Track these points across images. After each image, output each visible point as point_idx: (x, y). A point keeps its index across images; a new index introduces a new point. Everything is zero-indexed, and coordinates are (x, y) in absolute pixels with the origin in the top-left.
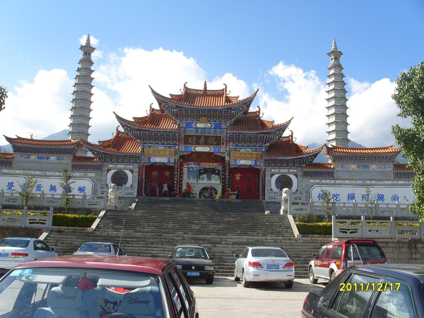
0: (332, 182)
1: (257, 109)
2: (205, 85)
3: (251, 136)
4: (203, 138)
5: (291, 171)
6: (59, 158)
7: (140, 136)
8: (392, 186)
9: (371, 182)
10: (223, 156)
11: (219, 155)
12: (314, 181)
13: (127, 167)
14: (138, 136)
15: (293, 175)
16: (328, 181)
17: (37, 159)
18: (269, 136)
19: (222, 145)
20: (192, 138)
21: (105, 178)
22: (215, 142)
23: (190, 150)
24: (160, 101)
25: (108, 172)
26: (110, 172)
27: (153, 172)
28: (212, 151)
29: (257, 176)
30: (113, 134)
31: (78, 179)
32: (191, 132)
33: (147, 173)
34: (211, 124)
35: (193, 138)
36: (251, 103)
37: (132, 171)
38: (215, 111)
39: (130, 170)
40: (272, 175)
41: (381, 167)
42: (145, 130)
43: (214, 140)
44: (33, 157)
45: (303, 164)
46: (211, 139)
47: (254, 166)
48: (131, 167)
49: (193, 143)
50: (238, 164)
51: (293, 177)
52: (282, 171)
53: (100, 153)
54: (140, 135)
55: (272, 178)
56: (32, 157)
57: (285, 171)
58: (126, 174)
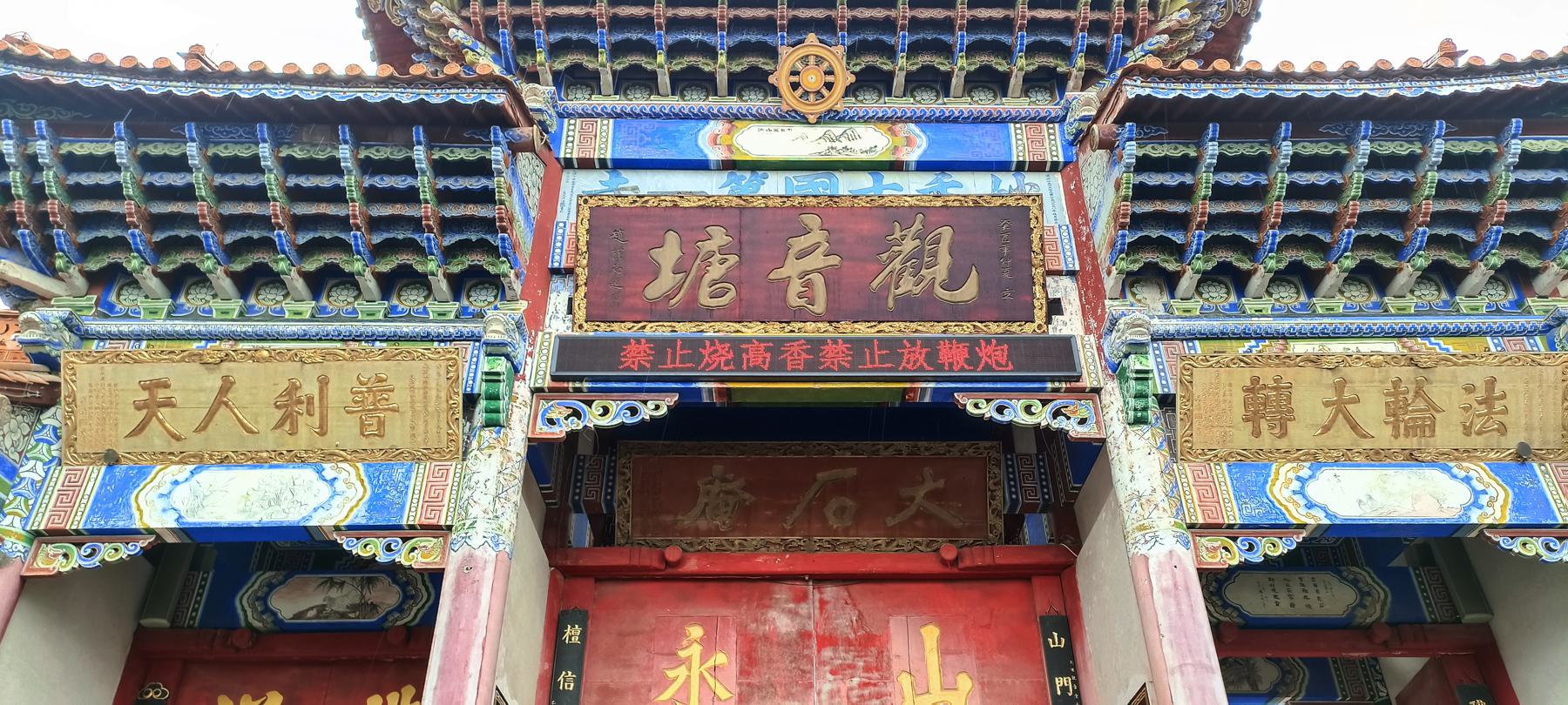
11: (1024, 419)
19: (1040, 314)
43: (944, 259)
46: (909, 245)
49: (705, 299)
54: (38, 193)
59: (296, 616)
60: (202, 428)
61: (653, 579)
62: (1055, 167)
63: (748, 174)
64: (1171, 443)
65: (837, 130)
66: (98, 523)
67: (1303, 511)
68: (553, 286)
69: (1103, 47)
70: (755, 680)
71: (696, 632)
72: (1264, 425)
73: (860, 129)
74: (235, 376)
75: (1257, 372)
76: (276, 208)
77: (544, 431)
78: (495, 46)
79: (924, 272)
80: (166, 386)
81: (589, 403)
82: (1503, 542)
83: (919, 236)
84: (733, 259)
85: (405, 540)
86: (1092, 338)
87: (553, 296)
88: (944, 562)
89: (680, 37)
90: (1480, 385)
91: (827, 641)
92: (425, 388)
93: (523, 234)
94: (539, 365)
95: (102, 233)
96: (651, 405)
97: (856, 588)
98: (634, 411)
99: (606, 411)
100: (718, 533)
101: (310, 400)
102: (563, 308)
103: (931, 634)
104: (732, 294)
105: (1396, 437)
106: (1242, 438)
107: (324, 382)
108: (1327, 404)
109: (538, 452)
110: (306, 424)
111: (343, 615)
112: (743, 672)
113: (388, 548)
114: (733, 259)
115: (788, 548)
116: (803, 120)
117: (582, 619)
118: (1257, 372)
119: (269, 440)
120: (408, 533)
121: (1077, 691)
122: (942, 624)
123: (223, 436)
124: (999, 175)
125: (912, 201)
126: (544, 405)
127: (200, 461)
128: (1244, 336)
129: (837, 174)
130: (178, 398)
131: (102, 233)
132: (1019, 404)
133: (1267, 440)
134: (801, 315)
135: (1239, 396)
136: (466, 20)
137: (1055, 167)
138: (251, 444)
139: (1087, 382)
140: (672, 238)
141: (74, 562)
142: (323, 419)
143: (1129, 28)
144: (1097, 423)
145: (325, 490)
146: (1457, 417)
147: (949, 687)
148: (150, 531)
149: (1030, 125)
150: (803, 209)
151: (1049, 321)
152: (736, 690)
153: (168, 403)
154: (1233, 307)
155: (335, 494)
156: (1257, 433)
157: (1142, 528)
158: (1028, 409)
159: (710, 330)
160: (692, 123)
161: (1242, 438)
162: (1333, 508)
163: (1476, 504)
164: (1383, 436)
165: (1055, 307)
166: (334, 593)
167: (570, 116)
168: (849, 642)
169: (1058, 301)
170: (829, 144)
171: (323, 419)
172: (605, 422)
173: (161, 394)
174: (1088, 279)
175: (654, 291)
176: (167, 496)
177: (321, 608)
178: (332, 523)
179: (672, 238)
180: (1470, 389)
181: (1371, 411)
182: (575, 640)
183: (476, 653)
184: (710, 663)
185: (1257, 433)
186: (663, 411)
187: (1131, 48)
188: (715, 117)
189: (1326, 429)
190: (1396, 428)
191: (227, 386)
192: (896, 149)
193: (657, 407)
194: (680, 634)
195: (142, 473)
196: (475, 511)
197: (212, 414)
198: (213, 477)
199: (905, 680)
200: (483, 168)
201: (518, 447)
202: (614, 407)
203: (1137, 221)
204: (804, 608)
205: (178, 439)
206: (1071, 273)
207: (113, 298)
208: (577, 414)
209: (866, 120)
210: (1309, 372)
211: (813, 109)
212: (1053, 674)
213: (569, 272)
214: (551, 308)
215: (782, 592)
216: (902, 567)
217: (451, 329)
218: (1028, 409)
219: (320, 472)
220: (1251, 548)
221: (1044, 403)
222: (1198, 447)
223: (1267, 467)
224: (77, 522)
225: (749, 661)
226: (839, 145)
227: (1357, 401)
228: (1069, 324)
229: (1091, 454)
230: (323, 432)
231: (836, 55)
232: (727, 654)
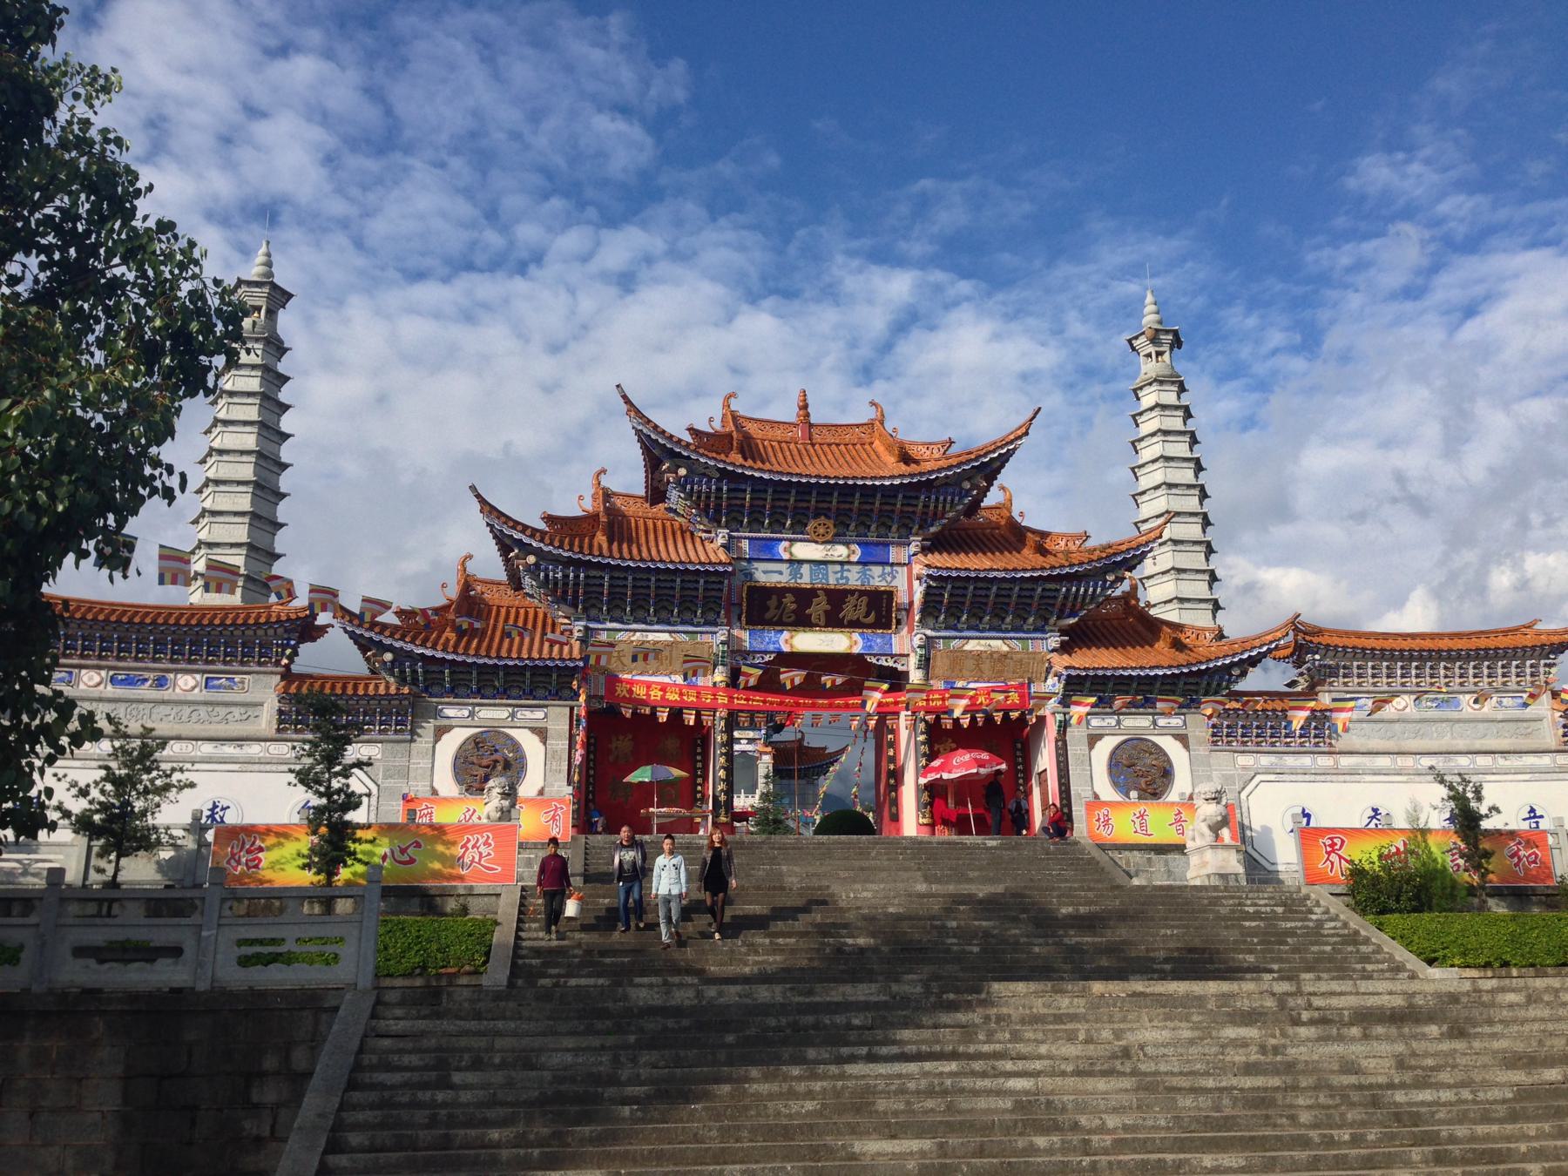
0: (1325, 761)
3: (1011, 589)
4: (822, 598)
5: (1162, 722)
6: (216, 682)
8: (1555, 776)
9: (1474, 762)
10: (900, 668)
11: (885, 664)
12: (1252, 762)
13: (519, 716)
15: (1170, 738)
16: (1306, 761)
17: (110, 687)
22: (867, 615)
23: (771, 647)
25: (1091, 745)
28: (856, 650)
30: (444, 586)
32: (768, 575)
36: (1002, 466)
37: (542, 733)
38: (869, 492)
39: (533, 730)
40: (1093, 740)
41: (1505, 701)
42: (599, 566)
44: (91, 679)
48: (539, 714)
49: (785, 619)
51: (530, 744)
52: (1128, 722)
53: (410, 654)
55: (1094, 753)
56: (85, 679)
57: (1143, 722)
58: (516, 747)
143: (935, 514)
231: (830, 523)
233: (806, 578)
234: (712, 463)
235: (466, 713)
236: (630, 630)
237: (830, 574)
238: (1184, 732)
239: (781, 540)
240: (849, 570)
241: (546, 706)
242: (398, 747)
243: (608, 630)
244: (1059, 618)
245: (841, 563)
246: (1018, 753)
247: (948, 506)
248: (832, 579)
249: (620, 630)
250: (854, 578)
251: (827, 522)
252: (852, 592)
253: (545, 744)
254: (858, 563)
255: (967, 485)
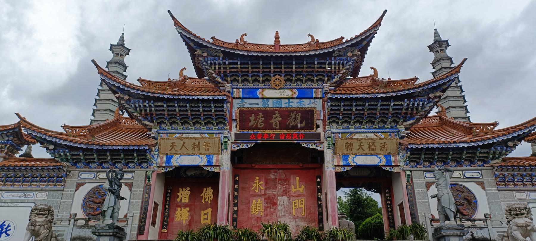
1: (372, 72)
2: (277, 38)
5: (468, 175)
7: (151, 115)
11: (311, 147)
14: (146, 115)
18: (413, 104)
19: (315, 128)
20: (256, 116)
21: (68, 202)
24: (191, 44)
26: (81, 188)
27: (181, 190)
29: (387, 191)
31: (6, 205)
33: (169, 191)
34: (292, 91)
35: (259, 117)
43: (299, 119)
45: (493, 159)
46: (294, 116)
47: (385, 166)
49: (259, 126)
50: (352, 164)
54: (151, 111)
59: (191, 175)
60: (181, 149)
61: (250, 169)
62: (321, 98)
63: (266, 100)
64: (334, 151)
65: (282, 91)
66: (167, 165)
67: (353, 163)
68: (233, 122)
69: (331, 75)
70: (268, 186)
71: (257, 178)
72: (348, 149)
73: (286, 90)
74: (185, 141)
75: (348, 141)
76: (189, 113)
77: (233, 149)
78: (220, 76)
79: (296, 121)
80: (175, 143)
81: (240, 144)
82: (383, 168)
83: (295, 115)
84: (263, 119)
85: (213, 167)
86: (324, 132)
87: (233, 124)
88: (300, 166)
89: (254, 74)
90: (383, 143)
91: (280, 179)
92: (215, 144)
93: (228, 116)
94: (232, 138)
95: (160, 116)
96: (250, 144)
97: (285, 170)
98: (248, 146)
99: (243, 146)
100: (261, 161)
101: (197, 145)
102: (235, 126)
103: (298, 178)
104: (263, 125)
105: (369, 151)
106: (345, 151)
107: (199, 143)
108: (358, 146)
109: (233, 153)
110: (197, 149)
111: (199, 175)
112: (265, 185)
113: (211, 169)
114: (263, 119)
115: (273, 164)
116: (276, 89)
117: (238, 176)
118: (348, 141)
119: (191, 151)
120: (214, 166)
121: (321, 188)
122: (299, 177)
123: (184, 151)
124: (311, 99)
125: (294, 109)
126: (233, 145)
127: (181, 155)
128: (348, 133)
129: (282, 99)
130: (177, 145)
131: (160, 116)
132: (310, 144)
133: (349, 152)
134: (275, 129)
135: (345, 145)
136: (216, 72)
137: (321, 98)
138: (188, 152)
139: (322, 141)
140: (253, 115)
141: (164, 171)
142: (199, 148)
143: (335, 72)
144: (323, 148)
145: (201, 160)
146: (379, 148)
147: (300, 187)
148: (175, 166)
149: (317, 89)
150: (276, 110)
151: (317, 129)
152: (264, 188)
153: (175, 146)
154: (348, 127)
155: (202, 160)
156: (347, 150)
157: (327, 166)
158: (312, 145)
159: (260, 132)
160: (256, 89)
161: (345, 151)
162: (357, 163)
163: (380, 162)
164: (367, 151)
165: (318, 126)
166: (196, 171)
167: (234, 89)
168: (283, 180)
169: (319, 125)
170: (281, 94)
171: (199, 148)
172: (243, 147)
173: (174, 144)
174: (324, 121)
175: (250, 124)
176: (177, 160)
177: (195, 174)
178: (202, 165)
179: (253, 115)
180: (381, 144)
181: (365, 147)
182: (237, 180)
183: (226, 185)
184: (260, 183)
185: (347, 150)
186: (252, 146)
187: (336, 76)
188: (260, 88)
189: (358, 150)
190: (369, 150)
191: (184, 143)
192: (292, 95)
193: (251, 145)
194: (255, 178)
195: (172, 156)
196: (224, 163)
197: (182, 147)
198: (183, 157)
199: (293, 186)
200: (223, 107)
201: (229, 152)
202: (244, 145)
203: (331, 114)
204: (276, 174)
205: (177, 151)
206: (322, 120)
207: (161, 126)
208: (238, 146)
209: (287, 89)
210: (356, 141)
211: (277, 87)
212: (237, 218)
213: (236, 120)
214: (233, 127)
215: (272, 171)
216: (293, 167)
217: (217, 132)
218: (312, 145)
219: (199, 156)
220: (344, 169)
221: (315, 144)
222: (338, 153)
223: (349, 156)
224: (164, 164)
225: (266, 183)
226: (282, 94)
227: (363, 145)
228: (320, 130)
229: (323, 152)
230: (199, 150)
231: (282, 78)
232: (263, 182)
233: (271, 104)
234: (218, 49)
235: (93, 176)
236: (181, 133)
237: (283, 104)
238: (482, 180)
239: (258, 89)
240: (292, 102)
241: (134, 171)
242: (56, 193)
243: (170, 133)
244: (404, 121)
245: (289, 98)
246: (387, 195)
247: (341, 66)
248: (284, 104)
249: (175, 133)
250: (295, 104)
251: (279, 77)
252: (292, 111)
253: (130, 190)
254: (297, 98)
255: (350, 54)
